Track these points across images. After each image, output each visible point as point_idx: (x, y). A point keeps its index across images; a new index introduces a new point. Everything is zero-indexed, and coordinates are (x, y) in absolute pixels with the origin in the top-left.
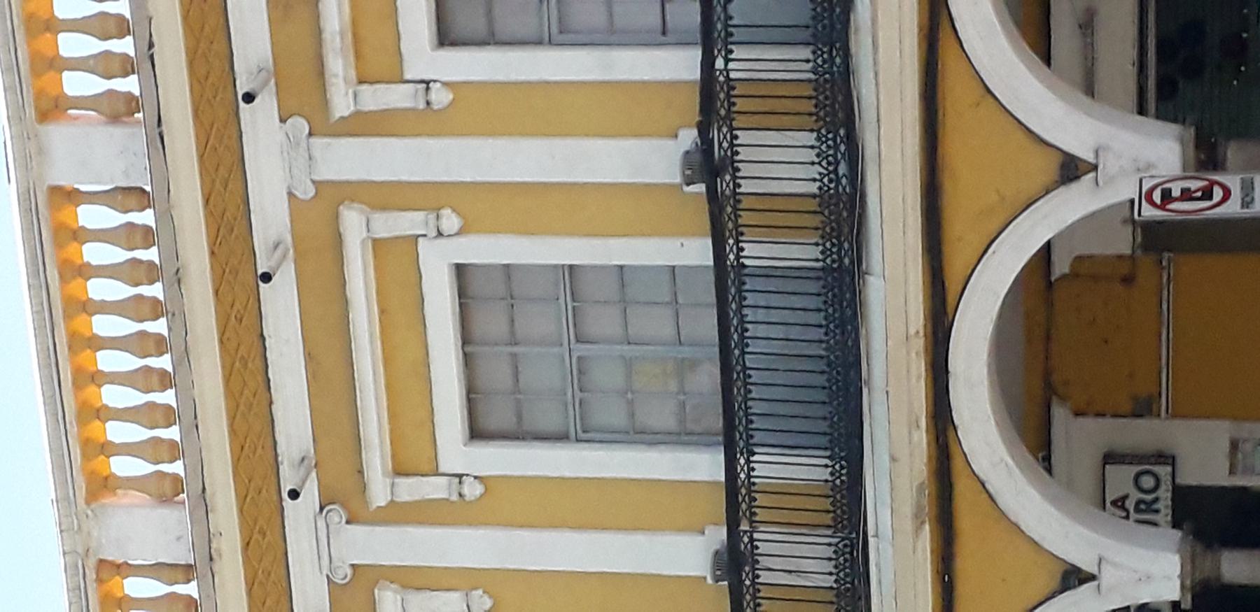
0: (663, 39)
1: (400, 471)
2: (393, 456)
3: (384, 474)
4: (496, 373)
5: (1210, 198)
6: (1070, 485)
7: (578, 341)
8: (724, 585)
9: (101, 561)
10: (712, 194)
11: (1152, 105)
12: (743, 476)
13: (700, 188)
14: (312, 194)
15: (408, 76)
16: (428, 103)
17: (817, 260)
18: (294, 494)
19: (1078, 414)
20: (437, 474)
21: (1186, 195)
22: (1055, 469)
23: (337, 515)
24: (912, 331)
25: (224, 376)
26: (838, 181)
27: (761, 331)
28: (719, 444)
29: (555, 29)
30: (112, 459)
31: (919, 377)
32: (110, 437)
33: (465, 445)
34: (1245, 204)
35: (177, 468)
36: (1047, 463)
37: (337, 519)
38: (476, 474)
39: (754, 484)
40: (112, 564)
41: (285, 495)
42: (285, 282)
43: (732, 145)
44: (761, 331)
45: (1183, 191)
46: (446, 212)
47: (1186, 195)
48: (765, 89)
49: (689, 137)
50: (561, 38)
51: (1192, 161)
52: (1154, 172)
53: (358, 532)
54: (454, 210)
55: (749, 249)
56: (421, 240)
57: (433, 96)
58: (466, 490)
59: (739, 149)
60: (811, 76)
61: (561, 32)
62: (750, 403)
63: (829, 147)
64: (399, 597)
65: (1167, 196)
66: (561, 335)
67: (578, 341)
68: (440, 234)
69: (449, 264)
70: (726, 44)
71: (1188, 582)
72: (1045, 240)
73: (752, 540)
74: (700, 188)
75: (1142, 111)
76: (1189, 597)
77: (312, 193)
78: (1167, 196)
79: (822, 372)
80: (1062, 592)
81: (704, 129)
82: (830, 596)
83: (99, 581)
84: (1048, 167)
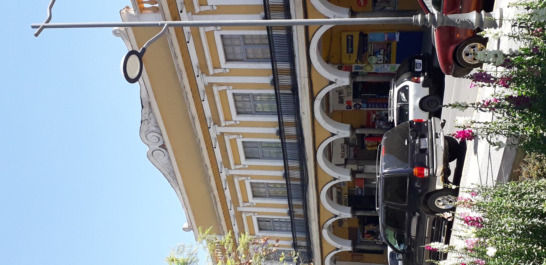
3: (212, 69)
4: (229, 50)
12: (275, 68)
18: (181, 12)
20: (233, 120)
22: (333, 200)
23: (216, 126)
25: (185, 69)
35: (157, 5)
55: (280, 91)
56: (214, 31)
57: (237, 123)
63: (286, 3)
64: (203, 28)
69: (253, 199)
73: (270, 16)
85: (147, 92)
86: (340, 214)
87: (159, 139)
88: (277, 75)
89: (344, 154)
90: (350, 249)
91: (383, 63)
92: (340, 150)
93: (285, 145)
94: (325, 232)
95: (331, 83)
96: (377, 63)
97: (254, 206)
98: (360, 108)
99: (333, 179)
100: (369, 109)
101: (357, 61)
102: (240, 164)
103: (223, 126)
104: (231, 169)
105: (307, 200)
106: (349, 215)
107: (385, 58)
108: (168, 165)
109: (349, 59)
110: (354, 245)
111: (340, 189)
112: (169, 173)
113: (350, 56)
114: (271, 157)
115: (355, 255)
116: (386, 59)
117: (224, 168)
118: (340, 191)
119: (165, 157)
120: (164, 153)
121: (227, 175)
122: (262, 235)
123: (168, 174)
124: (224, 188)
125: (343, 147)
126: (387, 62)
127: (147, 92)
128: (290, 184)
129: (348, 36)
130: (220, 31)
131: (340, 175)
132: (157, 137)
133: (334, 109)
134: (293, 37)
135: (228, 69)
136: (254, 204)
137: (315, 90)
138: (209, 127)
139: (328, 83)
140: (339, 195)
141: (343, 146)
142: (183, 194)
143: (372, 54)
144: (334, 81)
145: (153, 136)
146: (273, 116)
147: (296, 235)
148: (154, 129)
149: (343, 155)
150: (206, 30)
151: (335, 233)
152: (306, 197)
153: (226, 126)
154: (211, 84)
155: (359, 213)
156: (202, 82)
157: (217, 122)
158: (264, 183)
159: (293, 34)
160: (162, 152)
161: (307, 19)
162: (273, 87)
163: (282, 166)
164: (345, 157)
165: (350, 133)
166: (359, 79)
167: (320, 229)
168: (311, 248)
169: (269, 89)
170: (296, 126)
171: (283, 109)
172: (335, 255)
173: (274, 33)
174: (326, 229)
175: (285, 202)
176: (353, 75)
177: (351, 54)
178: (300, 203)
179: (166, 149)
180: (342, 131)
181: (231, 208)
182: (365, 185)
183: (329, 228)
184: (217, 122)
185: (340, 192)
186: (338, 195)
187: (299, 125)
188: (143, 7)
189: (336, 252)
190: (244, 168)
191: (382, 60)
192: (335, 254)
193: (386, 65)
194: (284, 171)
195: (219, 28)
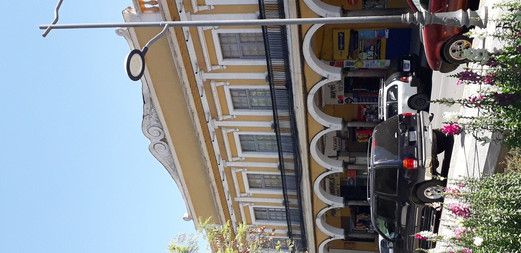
2: (211, 63)
4: (226, 47)
12: (270, 64)
23: (214, 120)
28: (281, 189)
30: (145, 5)
33: (234, 111)
35: (157, 5)
38: (213, 5)
46: (227, 82)
54: (228, 82)
56: (212, 30)
58: (234, 117)
61: (243, 56)
66: (238, 50)
79: (280, 30)
82: (280, 34)
84: (323, 128)
86: (333, 204)
87: (160, 133)
89: (337, 146)
94: (318, 221)
95: (324, 78)
96: (367, 59)
97: (250, 197)
98: (351, 102)
101: (348, 57)
102: (237, 157)
104: (229, 161)
106: (342, 205)
107: (375, 54)
108: (169, 157)
110: (346, 233)
117: (222, 160)
118: (333, 182)
119: (165, 150)
120: (165, 146)
121: (225, 166)
126: (377, 58)
128: (285, 175)
131: (334, 203)
134: (287, 35)
136: (251, 195)
137: (308, 86)
138: (207, 121)
139: (321, 79)
141: (335, 139)
143: (363, 51)
144: (326, 76)
148: (155, 123)
151: (327, 222)
152: (300, 188)
153: (223, 120)
155: (351, 203)
156: (200, 78)
158: (260, 174)
160: (163, 145)
161: (300, 18)
164: (337, 150)
168: (305, 236)
170: (290, 120)
173: (268, 31)
176: (345, 71)
179: (167, 143)
181: (224, 179)
184: (215, 117)
186: (330, 185)
189: (329, 240)
191: (372, 56)
193: (376, 61)
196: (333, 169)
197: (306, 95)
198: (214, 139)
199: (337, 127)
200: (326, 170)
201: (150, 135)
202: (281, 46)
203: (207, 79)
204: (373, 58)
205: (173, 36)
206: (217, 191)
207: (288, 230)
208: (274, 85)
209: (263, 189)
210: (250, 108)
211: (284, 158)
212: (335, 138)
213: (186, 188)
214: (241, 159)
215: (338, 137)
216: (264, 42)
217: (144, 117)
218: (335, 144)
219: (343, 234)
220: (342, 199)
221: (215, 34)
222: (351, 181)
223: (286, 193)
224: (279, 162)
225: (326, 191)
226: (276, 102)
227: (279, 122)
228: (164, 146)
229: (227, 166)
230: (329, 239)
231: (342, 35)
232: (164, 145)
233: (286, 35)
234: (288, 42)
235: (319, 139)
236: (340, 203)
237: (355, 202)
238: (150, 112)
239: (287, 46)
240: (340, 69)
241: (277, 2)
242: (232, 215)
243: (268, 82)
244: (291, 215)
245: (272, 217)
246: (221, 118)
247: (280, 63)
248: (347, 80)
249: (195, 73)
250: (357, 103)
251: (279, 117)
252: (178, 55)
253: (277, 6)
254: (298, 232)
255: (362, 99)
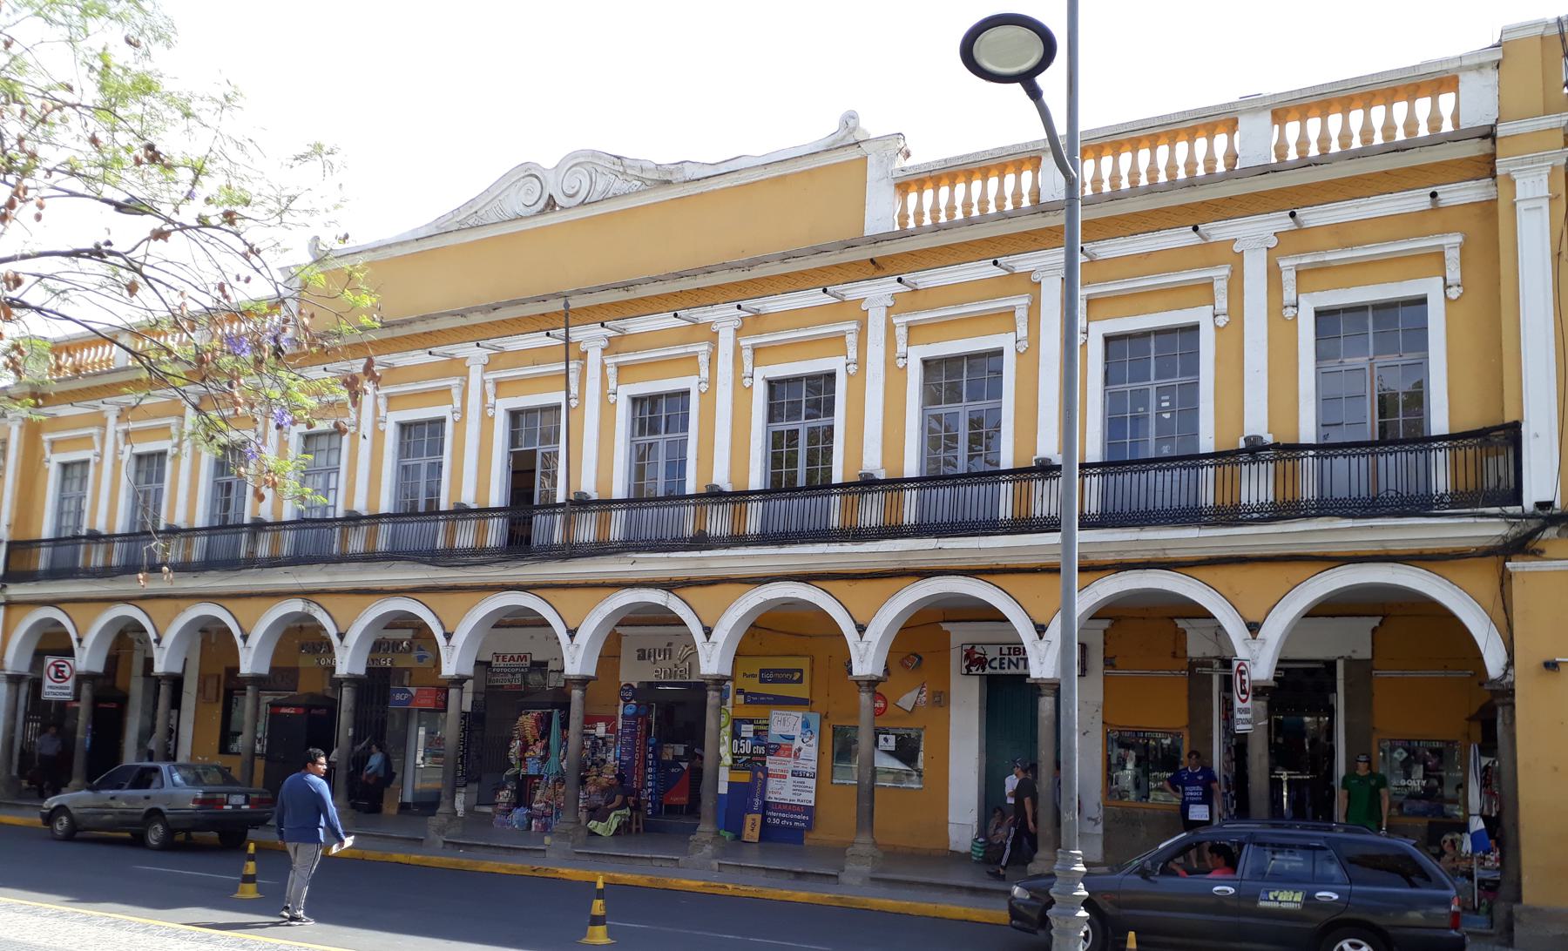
0: (1320, 424)
1: (910, 328)
5: (1242, 693)
6: (1085, 624)
7: (1157, 388)
8: (1126, 456)
9: (1041, 159)
10: (1239, 452)
11: (1282, 666)
13: (1242, 444)
14: (1236, 251)
15: (1300, 296)
16: (1286, 307)
17: (1437, 491)
19: (1105, 631)
21: (1243, 682)
22: (1091, 621)
24: (1167, 552)
26: (1249, 513)
27: (1168, 479)
28: (1104, 459)
29: (1324, 370)
31: (1143, 555)
32: (942, 188)
34: (1239, 709)
36: (1305, 616)
37: (736, 324)
39: (1298, 460)
40: (1040, 163)
41: (1433, 189)
42: (827, 299)
43: (1267, 460)
44: (1168, 479)
45: (1245, 680)
47: (1243, 682)
48: (900, 504)
49: (1269, 439)
50: (1107, 394)
51: (1257, 684)
52: (1252, 666)
53: (731, 333)
56: (1212, 307)
58: (747, 379)
59: (1265, 464)
60: (1305, 499)
62: (1178, 469)
65: (1242, 673)
67: (1157, 388)
68: (1215, 316)
70: (764, 500)
71: (1039, 681)
72: (1216, 616)
74: (1242, 444)
75: (1280, 661)
76: (1033, 682)
77: (863, 309)
78: (1242, 673)
80: (1034, 623)
81: (1276, 446)
83: (1031, 158)
85: (699, 180)
87: (572, 196)
88: (734, 502)
89: (503, 661)
90: (246, 667)
91: (733, 754)
92: (517, 650)
93: (549, 514)
94: (296, 606)
95: (708, 632)
97: (375, 424)
98: (623, 698)
99: (448, 630)
100: (620, 720)
102: (496, 396)
103: (603, 361)
104: (485, 372)
105: (392, 563)
106: (342, 669)
107: (745, 758)
108: (500, 212)
109: (745, 674)
110: (256, 680)
111: (408, 647)
112: (476, 212)
113: (754, 676)
114: (62, 514)
115: (219, 683)
116: (741, 761)
117: (488, 355)
118: (401, 648)
119: (522, 206)
120: (534, 204)
121: (468, 360)
122: (291, 441)
123: (474, 210)
124: (432, 350)
125: (522, 657)
127: (699, 180)
128: (438, 520)
129: (801, 671)
130: (845, 371)
131: (719, 647)
132: (577, 192)
133: (623, 638)
134: (826, 545)
135: (1297, 314)
136: (381, 424)
137: (692, 593)
138: (606, 324)
139: (860, 622)
140: (391, 649)
141: (526, 657)
142: (416, 244)
144: (712, 639)
145: (580, 182)
146: (627, 488)
147: (290, 529)
148: (600, 187)
149: (500, 658)
150: (1217, 285)
152: (399, 559)
153: (604, 367)
154: (713, 339)
155: (347, 696)
156: (723, 317)
157: (755, 323)
158: (339, 463)
159: (833, 544)
160: (536, 199)
161: (1079, 571)
162: (704, 491)
163: (281, 515)
164: (494, 662)
165: (574, 676)
166: (712, 697)
167: (306, 594)
168: (252, 568)
169: (697, 478)
170: (597, 543)
171: (645, 511)
172: (228, 631)
173: (1003, 486)
174: (304, 609)
175: (385, 505)
176: (719, 681)
177: (758, 678)
178: (115, 561)
179: (542, 212)
180: (580, 655)
181: (435, 355)
182: (416, 711)
183: (309, 617)
184: (611, 347)
185: (398, 649)
186: (391, 642)
187: (602, 549)
188: (1309, 115)
189: (236, 632)
190: (486, 405)
191: (739, 749)
192: (230, 630)
194: (474, 506)
195: (852, 369)
196: (713, 649)
197: (668, 585)
198: (554, 337)
199: (573, 663)
200: (448, 630)
201: (568, 167)
202: (1140, 506)
203: (717, 333)
204: (735, 752)
205: (833, 258)
206: (395, 335)
207: (269, 521)
208: (343, 526)
209: (396, 458)
210: (1107, 387)
211: (491, 521)
212: (528, 656)
213: (407, 250)
214: (612, 391)
215: (528, 665)
216: (1450, 435)
217: (618, 158)
218: (512, 656)
219: (255, 671)
220: (361, 670)
221: (1005, 342)
222: (403, 697)
223: (365, 524)
224: (476, 507)
225: (493, 627)
226: (412, 522)
227: (619, 513)
228: (533, 202)
229: (469, 367)
230: (335, 632)
231: (795, 678)
232: (536, 202)
233: (825, 542)
234: (809, 545)
235: (674, 613)
236: (254, 662)
237: (351, 705)
238: (632, 175)
239: (796, 543)
240: (880, 673)
241: (1089, 512)
242: (325, 369)
243: (452, 509)
244: (319, 533)
245: (66, 502)
246: (609, 361)
247: (753, 525)
248: (701, 687)
249: (430, 350)
250: (620, 713)
251: (744, 505)
252: (783, 266)
253: (899, 523)
254: (263, 550)
255: (631, 727)
